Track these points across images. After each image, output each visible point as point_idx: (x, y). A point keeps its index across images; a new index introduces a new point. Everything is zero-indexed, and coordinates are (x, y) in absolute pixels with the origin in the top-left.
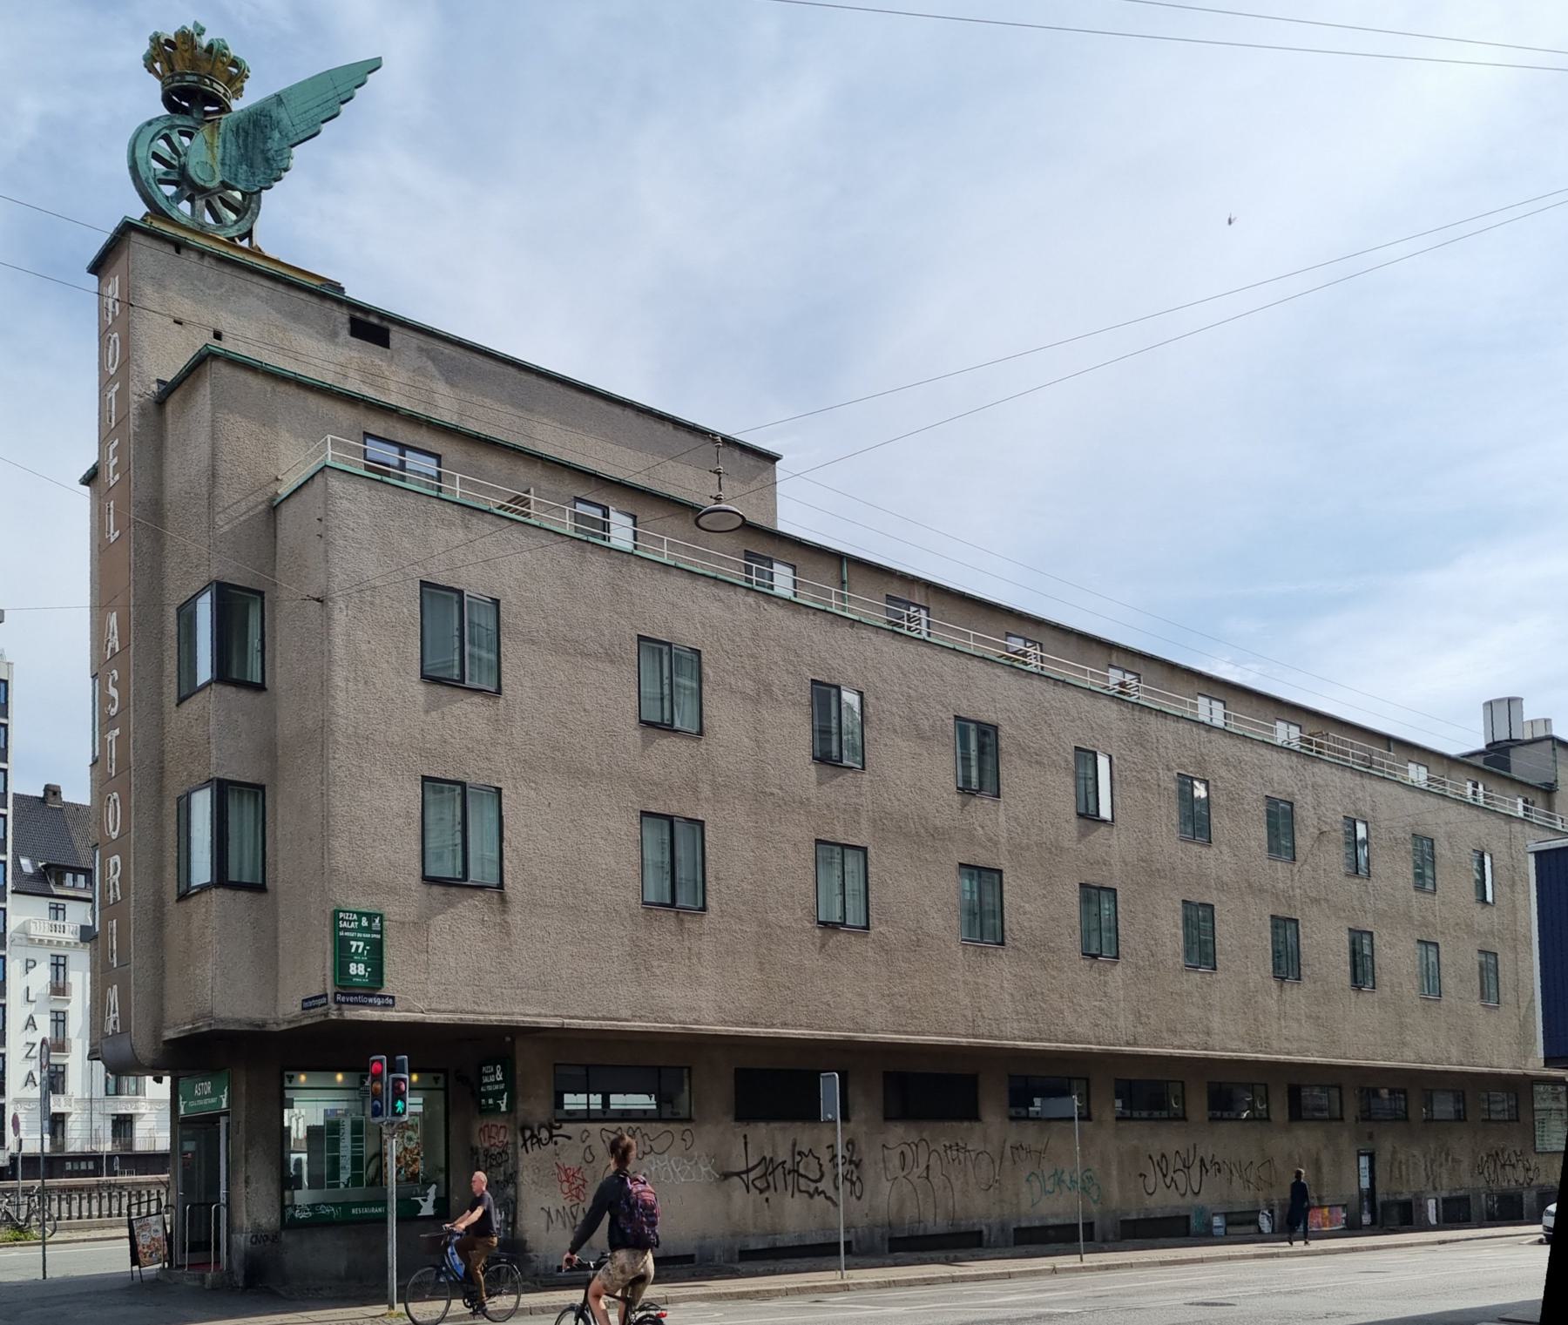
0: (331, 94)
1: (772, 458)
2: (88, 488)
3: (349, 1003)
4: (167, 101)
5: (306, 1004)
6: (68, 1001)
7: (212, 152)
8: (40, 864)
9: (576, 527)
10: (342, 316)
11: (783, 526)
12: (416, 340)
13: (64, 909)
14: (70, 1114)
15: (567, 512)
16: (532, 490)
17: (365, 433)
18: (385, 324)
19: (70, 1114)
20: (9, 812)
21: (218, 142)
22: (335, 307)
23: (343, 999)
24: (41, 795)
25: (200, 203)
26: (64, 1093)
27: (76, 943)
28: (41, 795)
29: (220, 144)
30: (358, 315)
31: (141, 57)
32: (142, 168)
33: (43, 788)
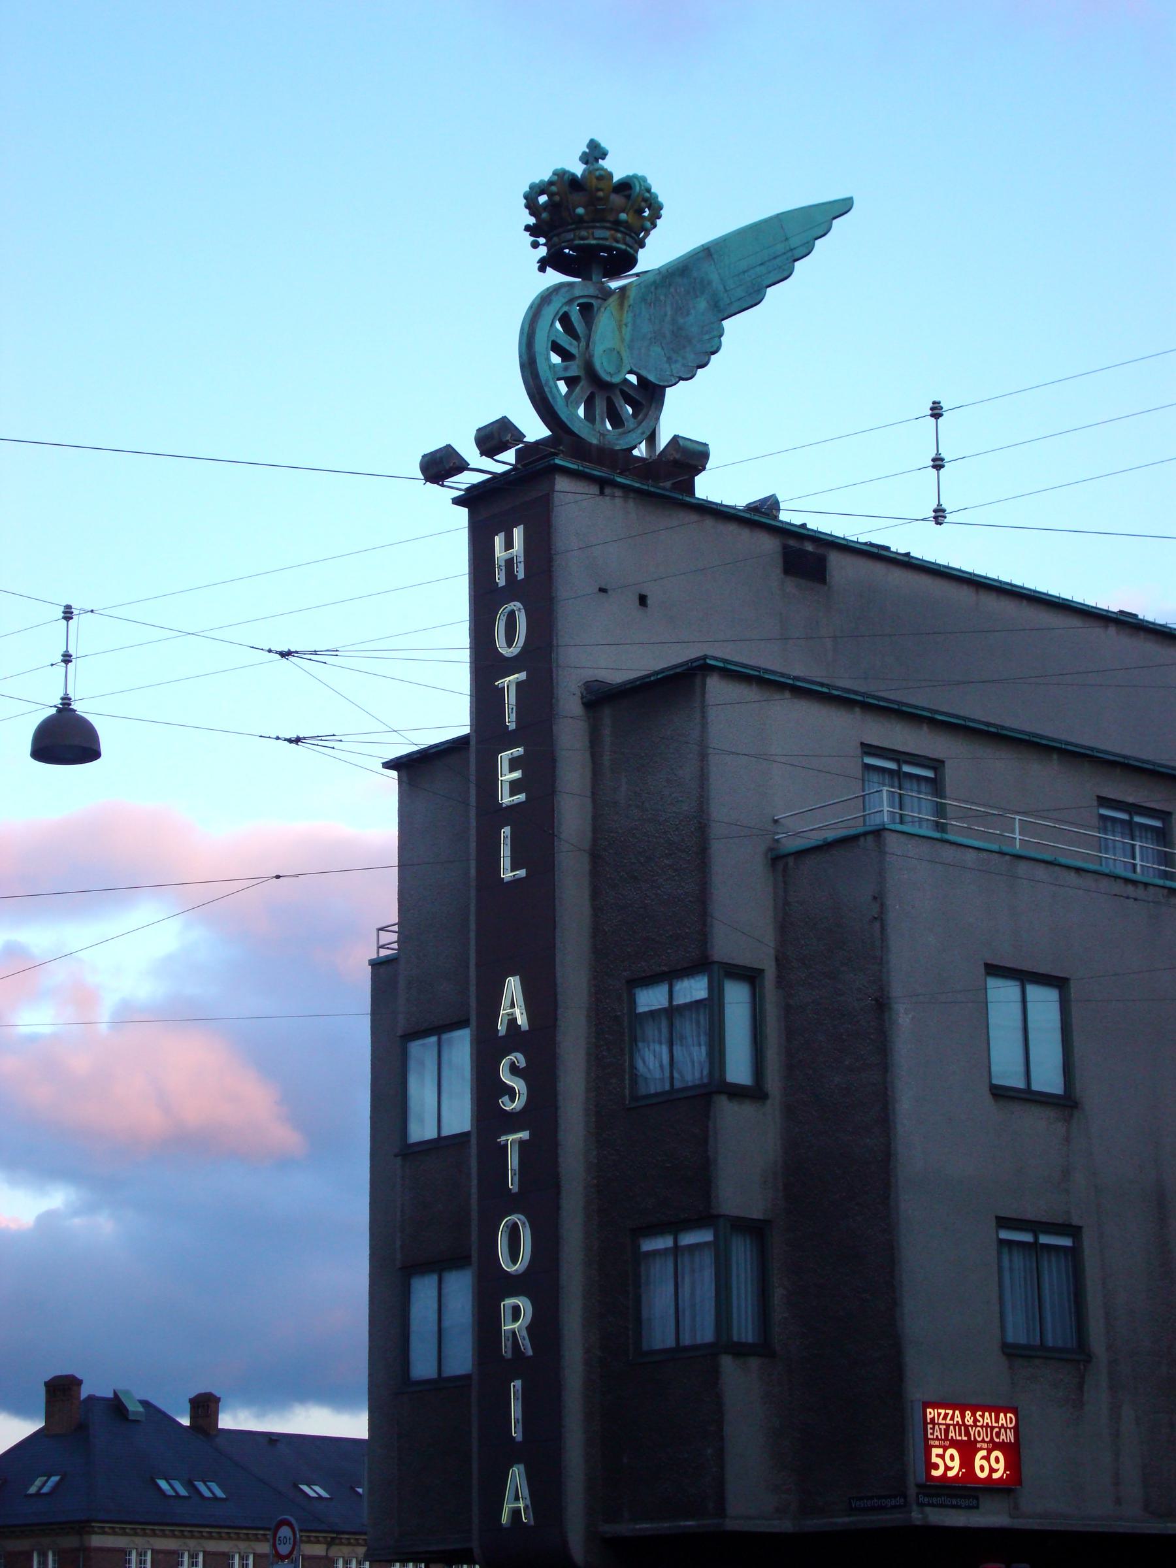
0: (780, 248)
3: (933, 1505)
7: (620, 332)
9: (937, 822)
15: (1018, 840)
21: (628, 317)
23: (926, 1499)
25: (600, 406)
29: (630, 320)
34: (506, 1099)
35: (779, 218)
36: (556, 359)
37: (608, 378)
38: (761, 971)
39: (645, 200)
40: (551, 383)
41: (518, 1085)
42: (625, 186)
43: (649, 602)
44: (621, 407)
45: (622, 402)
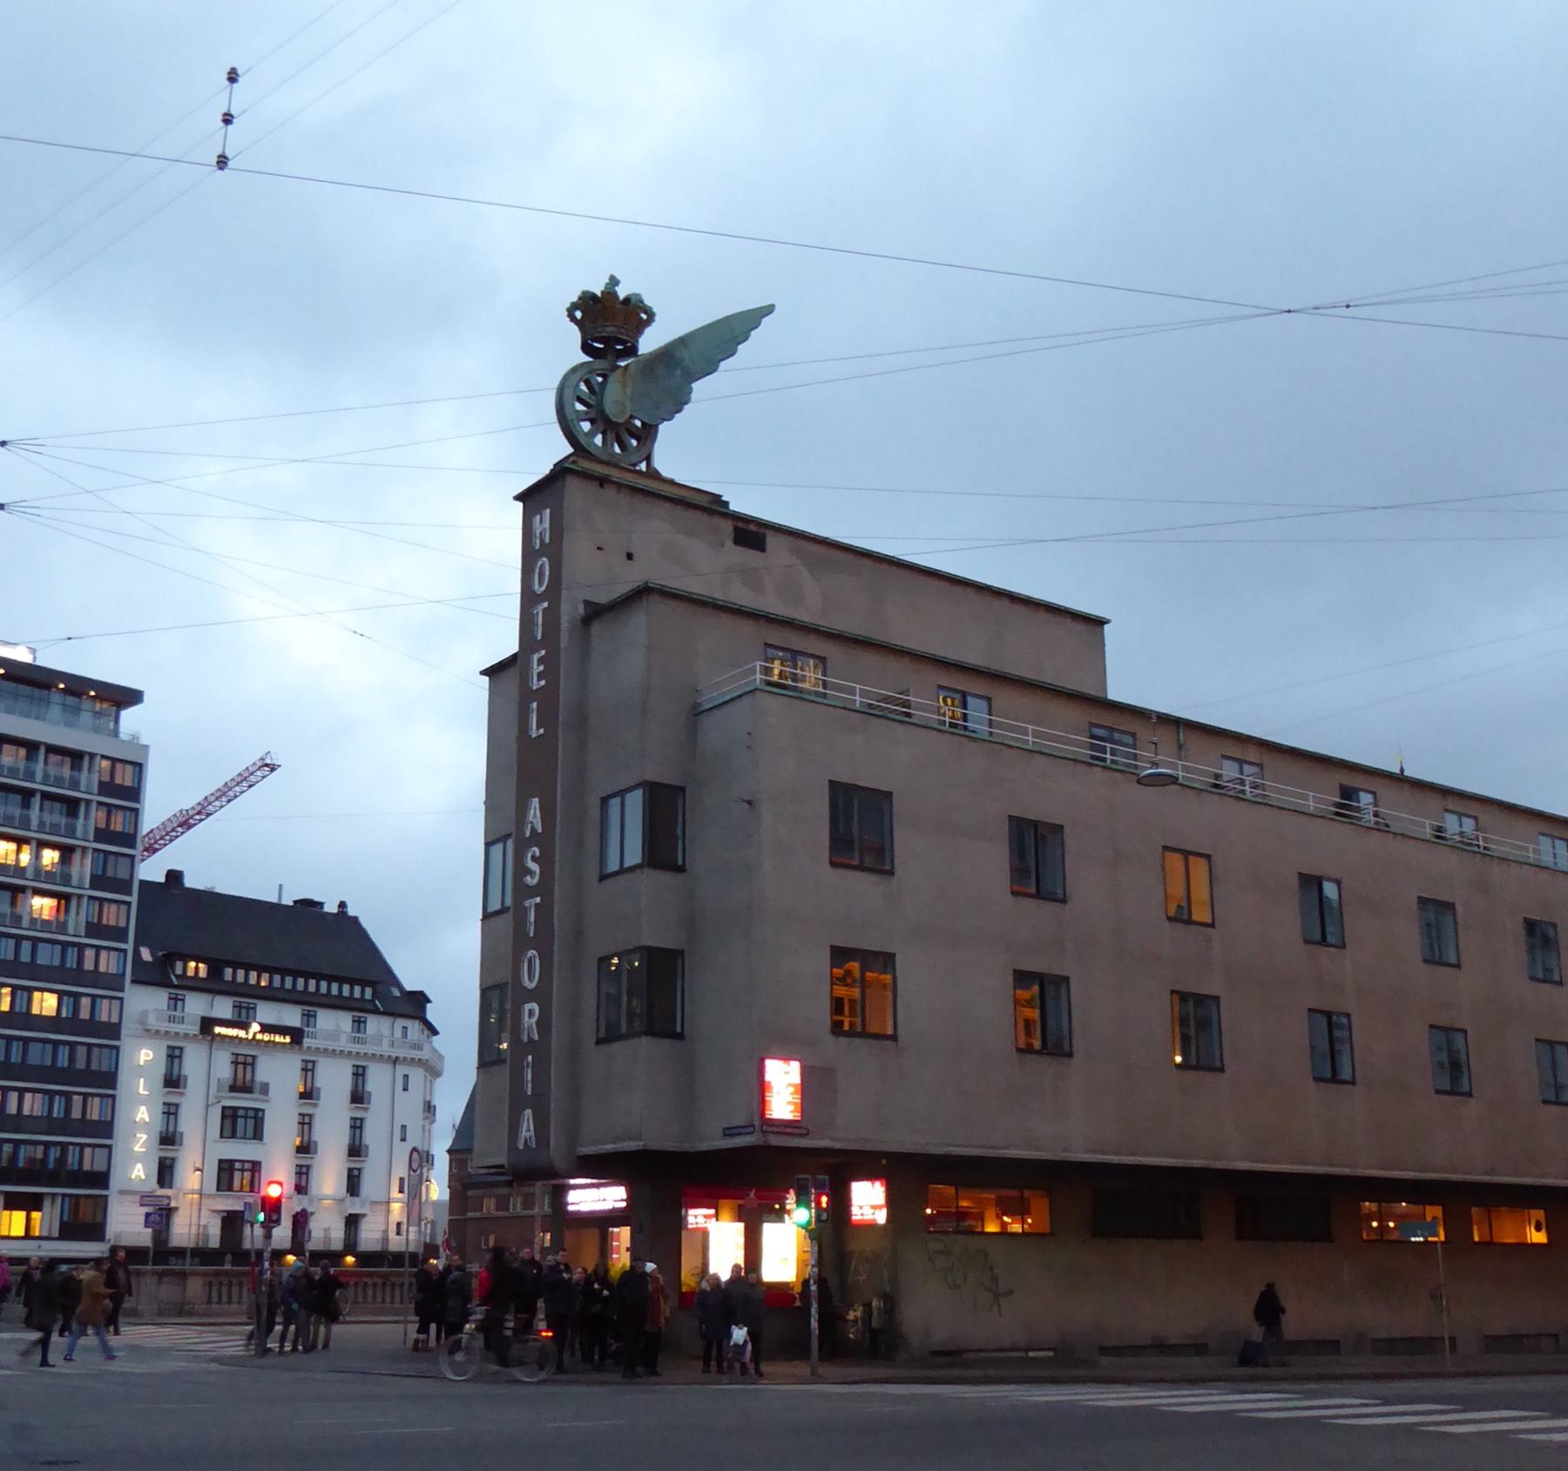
1: (1100, 623)
2: (487, 678)
4: (586, 348)
5: (727, 1132)
6: (366, 1109)
8: (160, 954)
10: (727, 527)
11: (1113, 695)
12: (783, 539)
13: (183, 1000)
14: (364, 1215)
16: (912, 690)
17: (765, 644)
18: (762, 530)
19: (364, 1215)
20: (134, 899)
22: (722, 520)
24: (162, 880)
25: (610, 436)
26: (306, 1194)
27: (195, 1035)
28: (162, 880)
30: (740, 524)
31: (565, 309)
32: (568, 412)
33: (165, 873)
34: (528, 878)
35: (727, 319)
36: (579, 407)
37: (614, 419)
38: (133, 982)
39: (640, 308)
40: (575, 422)
41: (535, 867)
42: (627, 300)
43: (625, 555)
44: (574, 426)
45: (627, 437)
